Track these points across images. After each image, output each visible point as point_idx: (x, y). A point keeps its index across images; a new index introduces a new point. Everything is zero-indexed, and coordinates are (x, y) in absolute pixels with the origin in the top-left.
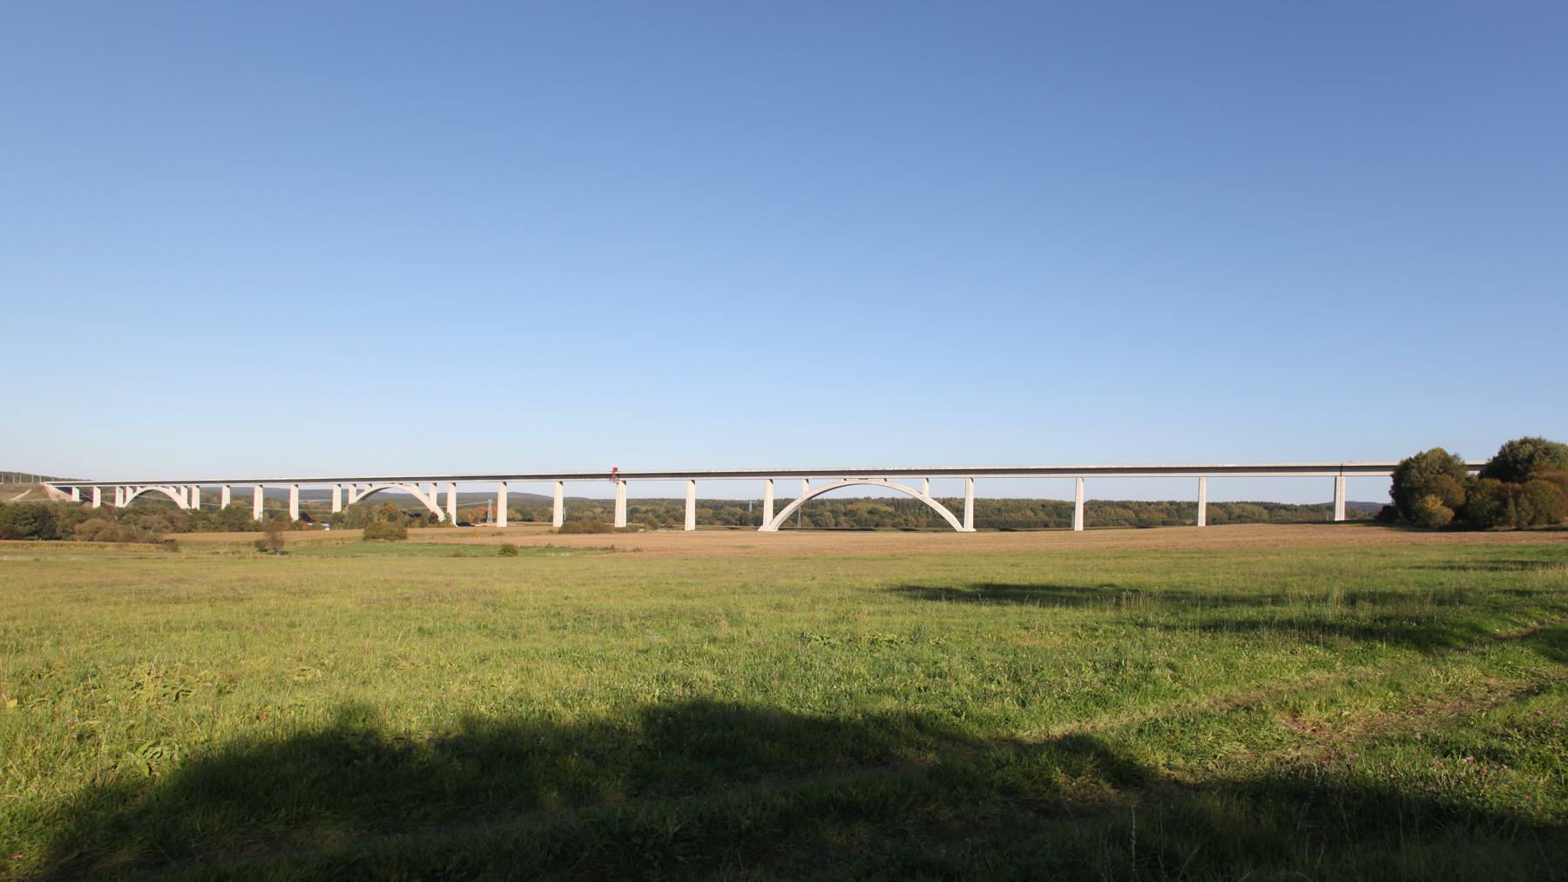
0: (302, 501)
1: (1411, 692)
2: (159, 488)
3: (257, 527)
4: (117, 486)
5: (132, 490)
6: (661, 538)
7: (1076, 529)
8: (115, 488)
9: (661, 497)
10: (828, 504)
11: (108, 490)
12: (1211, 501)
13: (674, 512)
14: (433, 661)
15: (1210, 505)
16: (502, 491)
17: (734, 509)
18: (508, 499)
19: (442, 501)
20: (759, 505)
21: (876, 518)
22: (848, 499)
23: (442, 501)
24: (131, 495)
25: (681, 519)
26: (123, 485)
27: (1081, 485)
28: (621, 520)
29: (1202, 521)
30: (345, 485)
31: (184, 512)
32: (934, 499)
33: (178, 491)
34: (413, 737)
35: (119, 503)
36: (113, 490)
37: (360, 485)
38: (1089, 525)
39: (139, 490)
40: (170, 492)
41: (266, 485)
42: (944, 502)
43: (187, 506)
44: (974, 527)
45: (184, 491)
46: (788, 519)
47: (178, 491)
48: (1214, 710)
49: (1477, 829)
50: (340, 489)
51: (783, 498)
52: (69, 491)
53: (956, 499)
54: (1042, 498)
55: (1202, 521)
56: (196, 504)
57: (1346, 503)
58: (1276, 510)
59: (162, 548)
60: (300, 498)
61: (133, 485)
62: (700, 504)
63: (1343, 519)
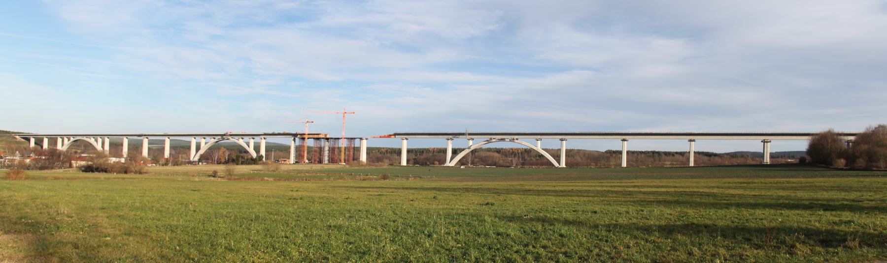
0: (150, 146)
2: (85, 138)
3: (253, 161)
4: (45, 137)
5: (61, 139)
8: (57, 138)
9: (653, 150)
10: (369, 151)
11: (53, 140)
16: (405, 145)
18: (254, 146)
19: (257, 148)
20: (444, 151)
22: (707, 152)
23: (257, 148)
26: (62, 136)
27: (405, 142)
30: (257, 139)
32: (543, 149)
33: (96, 141)
34: (103, 166)
35: (59, 147)
36: (42, 140)
37: (208, 138)
40: (92, 140)
42: (546, 150)
44: (566, 165)
45: (100, 140)
47: (96, 141)
48: (792, 213)
50: (147, 140)
52: (28, 140)
54: (712, 152)
58: (664, 157)
59: (838, 201)
60: (149, 144)
61: (68, 136)
62: (409, 151)
63: (693, 165)
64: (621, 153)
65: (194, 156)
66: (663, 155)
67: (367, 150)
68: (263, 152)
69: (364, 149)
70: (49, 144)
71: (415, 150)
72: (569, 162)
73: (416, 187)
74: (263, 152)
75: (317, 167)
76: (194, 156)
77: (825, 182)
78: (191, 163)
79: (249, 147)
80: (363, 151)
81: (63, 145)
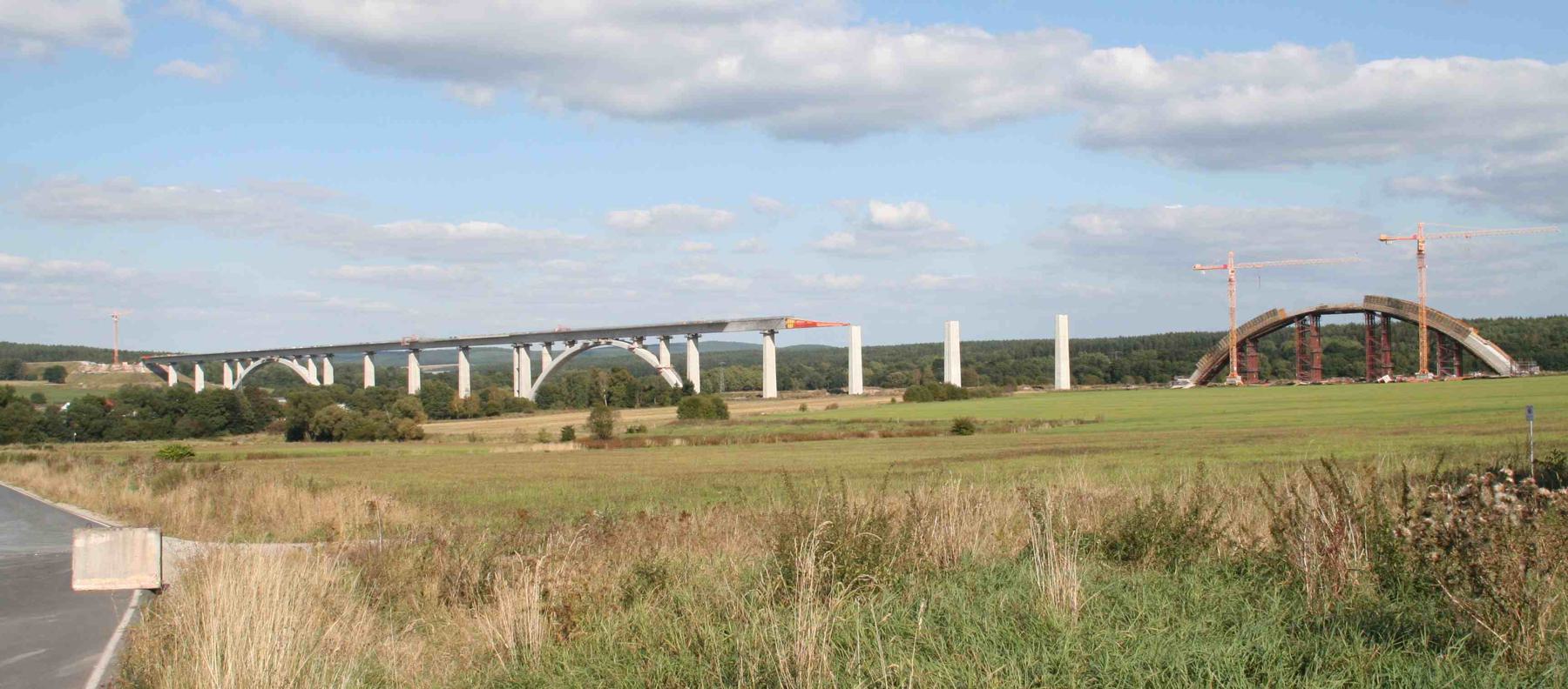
0: (425, 368)
1: (680, 609)
6: (1023, 401)
7: (1057, 387)
12: (965, 340)
13: (1002, 363)
14: (253, 551)
15: (1076, 347)
17: (1099, 355)
21: (1339, 357)
24: (242, 372)
25: (1049, 373)
28: (953, 374)
29: (1063, 377)
31: (315, 388)
38: (1077, 376)
39: (253, 365)
40: (294, 365)
41: (705, 337)
43: (317, 383)
46: (1476, 356)
49: (1298, 676)
51: (1164, 333)
53: (1555, 316)
55: (1063, 377)
56: (329, 380)
57: (962, 344)
64: (1046, 349)
65: (525, 389)
66: (946, 397)
67: (962, 353)
68: (694, 375)
69: (1061, 346)
70: (208, 378)
71: (1114, 344)
72: (588, 435)
73: (797, 443)
74: (694, 375)
75: (818, 404)
76: (525, 389)
77: (745, 675)
78: (518, 407)
79: (659, 360)
80: (952, 363)
81: (234, 379)
